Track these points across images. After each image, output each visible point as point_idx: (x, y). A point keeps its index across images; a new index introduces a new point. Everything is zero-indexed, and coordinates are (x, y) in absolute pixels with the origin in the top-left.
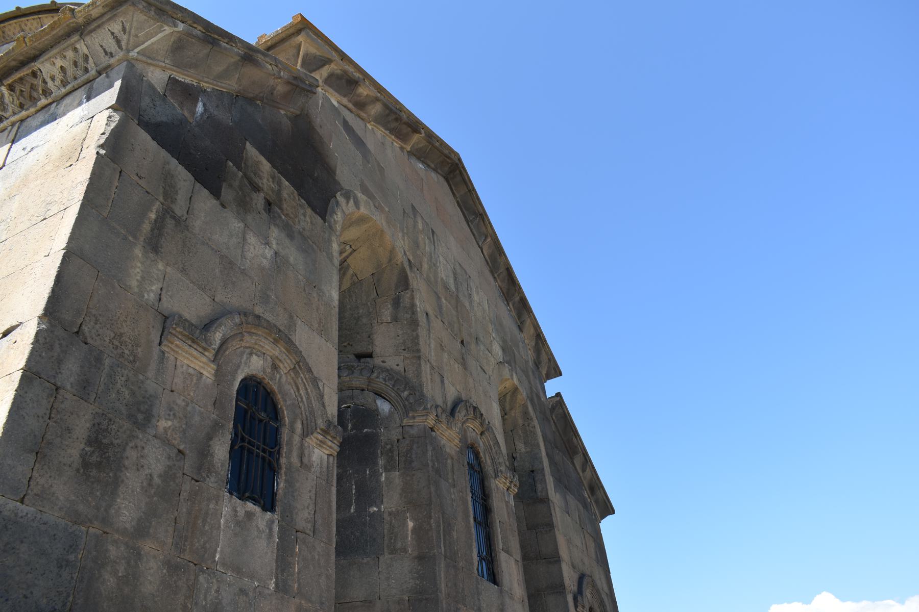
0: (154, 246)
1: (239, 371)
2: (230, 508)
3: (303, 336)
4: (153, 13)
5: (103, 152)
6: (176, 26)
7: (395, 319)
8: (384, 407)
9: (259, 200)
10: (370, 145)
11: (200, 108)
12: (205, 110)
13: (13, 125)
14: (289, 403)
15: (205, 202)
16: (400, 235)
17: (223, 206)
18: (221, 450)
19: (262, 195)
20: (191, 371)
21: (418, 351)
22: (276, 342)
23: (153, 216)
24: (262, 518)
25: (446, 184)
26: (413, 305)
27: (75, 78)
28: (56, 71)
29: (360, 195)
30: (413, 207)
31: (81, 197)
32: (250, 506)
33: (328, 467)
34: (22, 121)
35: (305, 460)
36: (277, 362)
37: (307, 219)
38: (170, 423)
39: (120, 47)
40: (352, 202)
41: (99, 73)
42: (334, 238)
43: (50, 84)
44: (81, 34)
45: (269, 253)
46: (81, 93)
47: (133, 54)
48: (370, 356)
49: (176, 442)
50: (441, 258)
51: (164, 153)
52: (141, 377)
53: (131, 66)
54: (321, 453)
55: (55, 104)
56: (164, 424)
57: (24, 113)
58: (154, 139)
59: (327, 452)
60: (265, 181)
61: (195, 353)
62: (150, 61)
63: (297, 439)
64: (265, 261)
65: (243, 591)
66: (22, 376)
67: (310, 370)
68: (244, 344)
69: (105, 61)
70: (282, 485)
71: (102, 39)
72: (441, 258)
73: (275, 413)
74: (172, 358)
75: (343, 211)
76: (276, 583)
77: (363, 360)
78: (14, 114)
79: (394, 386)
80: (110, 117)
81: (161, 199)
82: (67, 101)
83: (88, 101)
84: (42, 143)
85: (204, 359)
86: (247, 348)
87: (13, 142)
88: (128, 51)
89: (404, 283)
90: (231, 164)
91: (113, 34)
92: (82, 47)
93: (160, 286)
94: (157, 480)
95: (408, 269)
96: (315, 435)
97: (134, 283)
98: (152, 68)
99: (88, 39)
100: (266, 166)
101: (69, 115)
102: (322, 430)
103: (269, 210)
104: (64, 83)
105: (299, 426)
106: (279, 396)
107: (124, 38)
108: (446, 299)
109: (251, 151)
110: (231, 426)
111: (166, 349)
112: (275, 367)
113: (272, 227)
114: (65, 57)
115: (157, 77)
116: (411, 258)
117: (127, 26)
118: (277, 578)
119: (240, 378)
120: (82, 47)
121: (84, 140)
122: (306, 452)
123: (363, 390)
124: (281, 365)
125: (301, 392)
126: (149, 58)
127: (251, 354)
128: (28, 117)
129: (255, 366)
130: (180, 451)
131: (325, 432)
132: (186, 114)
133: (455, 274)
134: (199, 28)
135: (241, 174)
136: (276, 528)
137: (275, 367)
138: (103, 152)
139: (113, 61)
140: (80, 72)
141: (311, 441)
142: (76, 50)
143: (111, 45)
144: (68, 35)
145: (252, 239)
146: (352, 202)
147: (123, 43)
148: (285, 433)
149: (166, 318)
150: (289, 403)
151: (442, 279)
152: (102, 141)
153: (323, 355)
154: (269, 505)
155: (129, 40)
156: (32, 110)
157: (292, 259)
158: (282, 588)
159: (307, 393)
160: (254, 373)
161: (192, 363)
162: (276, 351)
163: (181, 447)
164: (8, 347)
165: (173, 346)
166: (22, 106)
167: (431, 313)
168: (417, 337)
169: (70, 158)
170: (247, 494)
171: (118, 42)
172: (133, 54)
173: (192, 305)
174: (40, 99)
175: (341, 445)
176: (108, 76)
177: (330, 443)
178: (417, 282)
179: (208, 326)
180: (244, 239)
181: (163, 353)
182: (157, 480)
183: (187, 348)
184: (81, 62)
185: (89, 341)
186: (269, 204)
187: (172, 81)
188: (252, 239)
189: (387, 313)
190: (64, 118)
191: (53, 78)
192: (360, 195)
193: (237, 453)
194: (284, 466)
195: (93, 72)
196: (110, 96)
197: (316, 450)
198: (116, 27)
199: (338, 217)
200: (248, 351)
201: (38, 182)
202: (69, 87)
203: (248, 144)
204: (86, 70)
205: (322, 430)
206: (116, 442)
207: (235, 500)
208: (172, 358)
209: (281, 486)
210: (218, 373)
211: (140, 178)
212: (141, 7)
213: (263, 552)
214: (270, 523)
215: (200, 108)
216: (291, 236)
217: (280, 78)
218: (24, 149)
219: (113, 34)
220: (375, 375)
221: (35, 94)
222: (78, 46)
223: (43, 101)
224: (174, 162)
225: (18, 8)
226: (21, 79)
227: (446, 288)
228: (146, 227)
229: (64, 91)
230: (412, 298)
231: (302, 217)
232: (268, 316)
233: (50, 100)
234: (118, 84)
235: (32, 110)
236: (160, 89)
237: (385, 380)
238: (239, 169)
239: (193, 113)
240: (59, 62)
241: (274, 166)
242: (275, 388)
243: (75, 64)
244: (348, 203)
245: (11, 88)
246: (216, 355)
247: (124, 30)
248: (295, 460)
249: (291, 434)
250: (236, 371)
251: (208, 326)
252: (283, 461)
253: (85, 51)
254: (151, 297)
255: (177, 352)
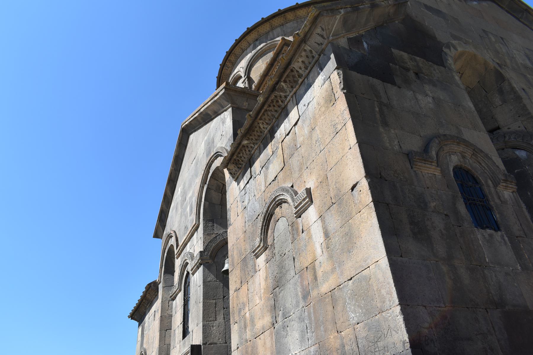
0: (385, 124)
1: (450, 166)
2: (481, 235)
3: (468, 135)
4: (330, 14)
5: (345, 91)
6: (340, 13)
7: (504, 101)
8: (522, 154)
9: (411, 75)
10: (444, 11)
11: (365, 45)
12: (368, 44)
13: (292, 97)
14: (479, 172)
15: (392, 90)
16: (485, 51)
17: (399, 87)
18: (462, 208)
19: (411, 71)
20: (430, 175)
21: (529, 113)
22: (458, 144)
23: (377, 109)
24: (498, 236)
25: (494, 4)
26: (513, 89)
27: (310, 63)
28: (300, 64)
29: (454, 42)
30: (484, 31)
31: (349, 116)
32: (489, 231)
33: (515, 199)
34: (295, 93)
35: (502, 199)
36: (464, 154)
37: (437, 72)
38: (435, 203)
39: (324, 38)
40: (452, 49)
41: (320, 55)
42: (454, 74)
43: (300, 71)
44: (305, 42)
45: (430, 100)
46: (316, 68)
47: (331, 38)
48: (498, 128)
49: (442, 211)
50: (515, 52)
51: (365, 77)
52: (413, 187)
53: (332, 44)
54: (508, 193)
55: (306, 79)
56: (433, 204)
57: (295, 90)
58: (358, 73)
59: (511, 191)
60: (409, 63)
61: (428, 166)
62: (338, 37)
63: (492, 190)
64: (430, 105)
65: (507, 274)
66: (374, 204)
67: (482, 151)
68: (445, 152)
69: (319, 48)
70: (498, 216)
71: (315, 39)
72: (515, 52)
73: (476, 181)
74: (420, 172)
75: (450, 55)
76: (520, 266)
77: (495, 133)
78: (291, 92)
79: (523, 140)
80: (338, 74)
81: (376, 99)
82: (311, 75)
83: (322, 70)
84: (311, 99)
85: (434, 167)
86: (446, 153)
87: (297, 104)
88: (328, 38)
89: (500, 77)
90: (391, 64)
91: (318, 34)
92: (308, 48)
93: (397, 141)
94: (444, 232)
95: (499, 69)
96: (501, 184)
97: (388, 145)
98: (339, 40)
99: (308, 43)
100: (405, 55)
101: (316, 81)
102: (503, 180)
103: (419, 78)
104: (306, 68)
105: (490, 182)
106: (473, 171)
107: (324, 33)
108: (530, 75)
109: (395, 51)
110: (460, 195)
111: (415, 169)
112: (464, 157)
113: (424, 85)
114: (302, 56)
115: (343, 42)
116: (498, 61)
117: (323, 27)
118: (519, 263)
119: (451, 169)
120: (308, 48)
121: (332, 89)
122: (500, 194)
123: (503, 149)
124: (466, 155)
125: (483, 164)
126: (337, 35)
127: (450, 155)
128: (297, 90)
129: (455, 160)
130: (446, 215)
131: (506, 181)
132: (362, 52)
133: (527, 56)
134: (348, 6)
135: (397, 66)
136: (506, 239)
137: (464, 157)
138: (345, 91)
139: (323, 46)
140: (311, 60)
141: (500, 188)
142: (305, 50)
143: (319, 39)
144: (299, 46)
145: (420, 97)
146: (452, 49)
147: (325, 36)
148: (486, 190)
149: (408, 155)
150: (479, 172)
151: (521, 64)
152: (342, 86)
153: (482, 140)
154: (497, 228)
155: (326, 33)
156: (297, 87)
157: (442, 97)
158: (525, 268)
159: (487, 164)
160: (456, 164)
161: (429, 171)
162: (461, 148)
163: (445, 213)
164: (359, 194)
165: (418, 167)
166: (292, 87)
167: (525, 87)
168: (525, 106)
169: (331, 99)
170: (485, 226)
171: (322, 36)
172: (331, 38)
173: (414, 144)
174: (298, 80)
175: (517, 185)
176: (324, 55)
177: (511, 186)
178: (509, 74)
179: (426, 149)
180: (417, 99)
181: (415, 171)
182: (444, 232)
183: (424, 165)
184: (309, 54)
185: (387, 179)
186: (416, 74)
187: (349, 39)
188: (420, 97)
189: (497, 100)
190: (315, 83)
191: (300, 68)
192: (454, 42)
193: (470, 205)
194: (494, 206)
195: (317, 56)
196: (332, 63)
197: (505, 192)
198: (319, 30)
199: (450, 61)
200: (448, 154)
201: (322, 118)
202: (309, 69)
203: (392, 49)
204: (313, 57)
205: (503, 180)
206: (420, 220)
207: (481, 230)
208: (420, 172)
209: (497, 216)
210: (442, 171)
211: (363, 94)
212: (325, 14)
213: (506, 252)
214: (502, 237)
215: (365, 45)
216: (435, 85)
217: (390, 5)
218: (304, 105)
219: (318, 34)
220: (507, 138)
221: (296, 79)
222: (305, 48)
223: (300, 80)
224: (371, 78)
225: (236, 40)
226: (287, 75)
227: (526, 67)
228: (378, 116)
229: (307, 71)
230: (510, 84)
231: (434, 72)
232: (447, 132)
233: (303, 78)
234: (332, 56)
235: (297, 87)
236: (347, 47)
237: (515, 138)
238: (396, 65)
239: (364, 49)
240: (300, 60)
241: (409, 53)
242: (469, 167)
243: (307, 57)
244: (450, 50)
245: (285, 82)
246: (437, 163)
247: (323, 29)
248: (497, 201)
249: (489, 188)
250: (448, 166)
251: (426, 149)
252: (492, 203)
253: (310, 48)
254: (397, 148)
255: (420, 169)
